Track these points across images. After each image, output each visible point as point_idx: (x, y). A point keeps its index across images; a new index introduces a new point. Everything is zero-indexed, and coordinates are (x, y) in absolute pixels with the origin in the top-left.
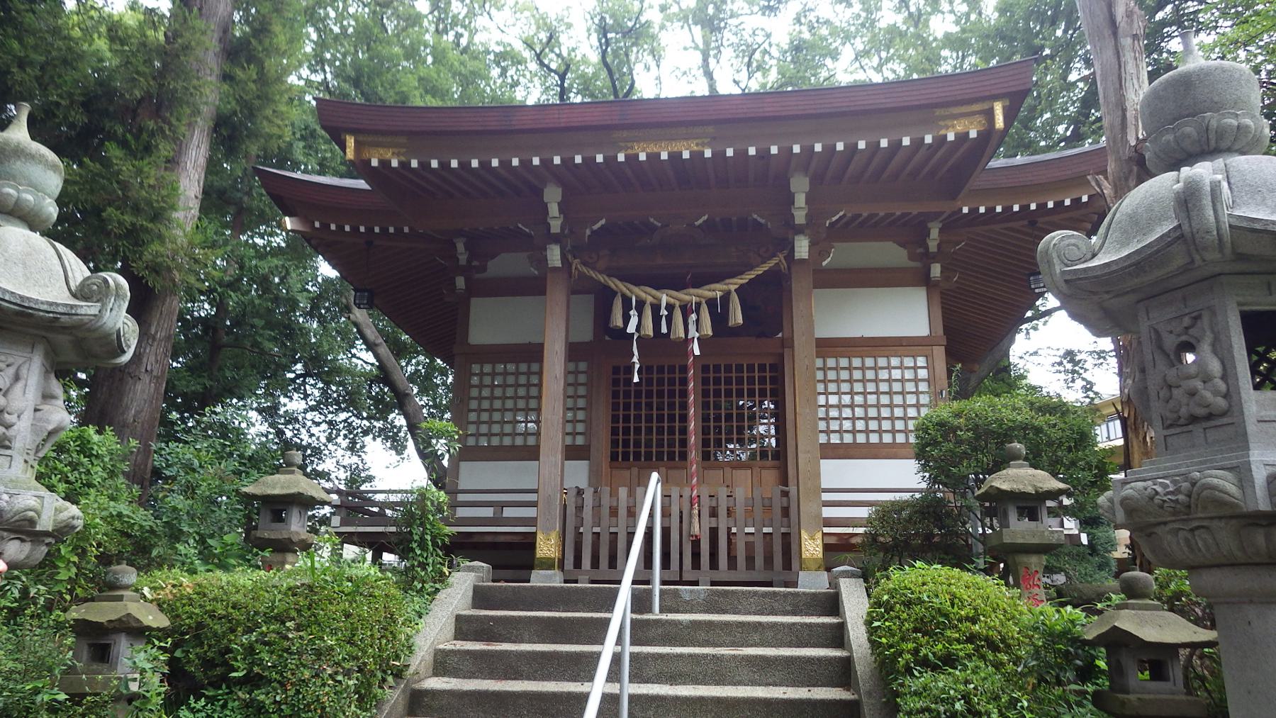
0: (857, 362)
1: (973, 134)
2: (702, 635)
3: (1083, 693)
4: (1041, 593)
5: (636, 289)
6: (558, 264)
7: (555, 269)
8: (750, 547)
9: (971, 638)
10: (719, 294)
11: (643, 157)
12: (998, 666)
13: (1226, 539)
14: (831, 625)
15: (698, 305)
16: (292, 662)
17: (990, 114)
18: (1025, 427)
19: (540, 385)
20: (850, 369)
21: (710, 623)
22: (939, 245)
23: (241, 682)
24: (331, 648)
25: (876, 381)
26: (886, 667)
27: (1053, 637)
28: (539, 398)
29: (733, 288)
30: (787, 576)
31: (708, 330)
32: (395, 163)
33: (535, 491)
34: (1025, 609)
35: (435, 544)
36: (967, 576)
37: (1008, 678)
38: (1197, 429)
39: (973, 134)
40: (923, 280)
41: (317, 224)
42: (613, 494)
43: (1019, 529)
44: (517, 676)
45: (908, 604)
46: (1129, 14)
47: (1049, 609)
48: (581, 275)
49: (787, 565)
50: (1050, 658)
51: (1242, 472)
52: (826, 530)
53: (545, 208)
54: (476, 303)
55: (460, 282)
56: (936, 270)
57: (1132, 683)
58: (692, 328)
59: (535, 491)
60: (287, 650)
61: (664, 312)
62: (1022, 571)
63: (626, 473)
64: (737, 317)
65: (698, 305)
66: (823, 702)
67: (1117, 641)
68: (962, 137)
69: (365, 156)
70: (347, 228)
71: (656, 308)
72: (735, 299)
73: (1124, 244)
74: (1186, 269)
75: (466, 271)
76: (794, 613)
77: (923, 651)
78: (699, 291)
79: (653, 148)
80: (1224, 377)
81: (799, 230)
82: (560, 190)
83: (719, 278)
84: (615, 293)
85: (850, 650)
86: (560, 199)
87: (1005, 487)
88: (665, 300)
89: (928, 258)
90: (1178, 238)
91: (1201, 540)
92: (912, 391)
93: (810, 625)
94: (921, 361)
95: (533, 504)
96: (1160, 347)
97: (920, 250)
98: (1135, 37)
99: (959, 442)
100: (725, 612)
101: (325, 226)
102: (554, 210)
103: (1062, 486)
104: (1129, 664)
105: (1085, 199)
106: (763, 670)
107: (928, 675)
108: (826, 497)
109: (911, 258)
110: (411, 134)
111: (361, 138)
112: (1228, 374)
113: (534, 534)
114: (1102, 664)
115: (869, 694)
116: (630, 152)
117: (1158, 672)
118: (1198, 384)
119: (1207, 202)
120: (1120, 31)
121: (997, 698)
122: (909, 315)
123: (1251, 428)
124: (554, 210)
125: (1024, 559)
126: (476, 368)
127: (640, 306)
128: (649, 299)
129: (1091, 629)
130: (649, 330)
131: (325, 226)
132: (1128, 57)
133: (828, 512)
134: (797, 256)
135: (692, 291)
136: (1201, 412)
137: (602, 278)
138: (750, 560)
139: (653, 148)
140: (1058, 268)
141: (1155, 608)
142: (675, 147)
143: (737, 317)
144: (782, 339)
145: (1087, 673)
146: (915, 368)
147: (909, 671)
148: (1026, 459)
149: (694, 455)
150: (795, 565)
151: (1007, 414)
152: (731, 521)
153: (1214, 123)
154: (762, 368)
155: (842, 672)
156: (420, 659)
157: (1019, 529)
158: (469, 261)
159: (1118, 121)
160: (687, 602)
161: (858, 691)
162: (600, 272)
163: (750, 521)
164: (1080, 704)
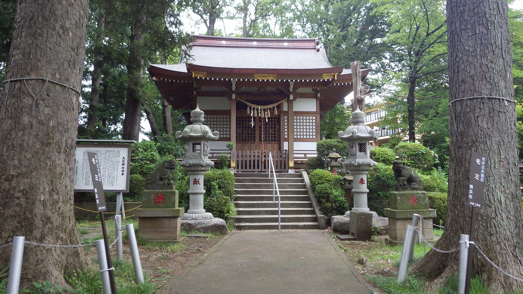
17: (334, 76)
18: (336, 146)
26: (313, 185)
30: (285, 170)
32: (203, 78)
40: (316, 97)
43: (334, 163)
47: (337, 176)
49: (285, 168)
51: (355, 161)
55: (195, 93)
61: (259, 111)
67: (345, 180)
69: (196, 76)
71: (258, 110)
72: (276, 109)
84: (247, 106)
88: (260, 108)
90: (351, 136)
94: (314, 118)
101: (164, 79)
108: (295, 152)
122: (310, 106)
127: (254, 109)
129: (342, 178)
131: (164, 79)
132: (358, 80)
133: (295, 156)
146: (312, 119)
149: (257, 139)
150: (287, 168)
151: (333, 143)
155: (304, 186)
157: (334, 163)
161: (307, 188)
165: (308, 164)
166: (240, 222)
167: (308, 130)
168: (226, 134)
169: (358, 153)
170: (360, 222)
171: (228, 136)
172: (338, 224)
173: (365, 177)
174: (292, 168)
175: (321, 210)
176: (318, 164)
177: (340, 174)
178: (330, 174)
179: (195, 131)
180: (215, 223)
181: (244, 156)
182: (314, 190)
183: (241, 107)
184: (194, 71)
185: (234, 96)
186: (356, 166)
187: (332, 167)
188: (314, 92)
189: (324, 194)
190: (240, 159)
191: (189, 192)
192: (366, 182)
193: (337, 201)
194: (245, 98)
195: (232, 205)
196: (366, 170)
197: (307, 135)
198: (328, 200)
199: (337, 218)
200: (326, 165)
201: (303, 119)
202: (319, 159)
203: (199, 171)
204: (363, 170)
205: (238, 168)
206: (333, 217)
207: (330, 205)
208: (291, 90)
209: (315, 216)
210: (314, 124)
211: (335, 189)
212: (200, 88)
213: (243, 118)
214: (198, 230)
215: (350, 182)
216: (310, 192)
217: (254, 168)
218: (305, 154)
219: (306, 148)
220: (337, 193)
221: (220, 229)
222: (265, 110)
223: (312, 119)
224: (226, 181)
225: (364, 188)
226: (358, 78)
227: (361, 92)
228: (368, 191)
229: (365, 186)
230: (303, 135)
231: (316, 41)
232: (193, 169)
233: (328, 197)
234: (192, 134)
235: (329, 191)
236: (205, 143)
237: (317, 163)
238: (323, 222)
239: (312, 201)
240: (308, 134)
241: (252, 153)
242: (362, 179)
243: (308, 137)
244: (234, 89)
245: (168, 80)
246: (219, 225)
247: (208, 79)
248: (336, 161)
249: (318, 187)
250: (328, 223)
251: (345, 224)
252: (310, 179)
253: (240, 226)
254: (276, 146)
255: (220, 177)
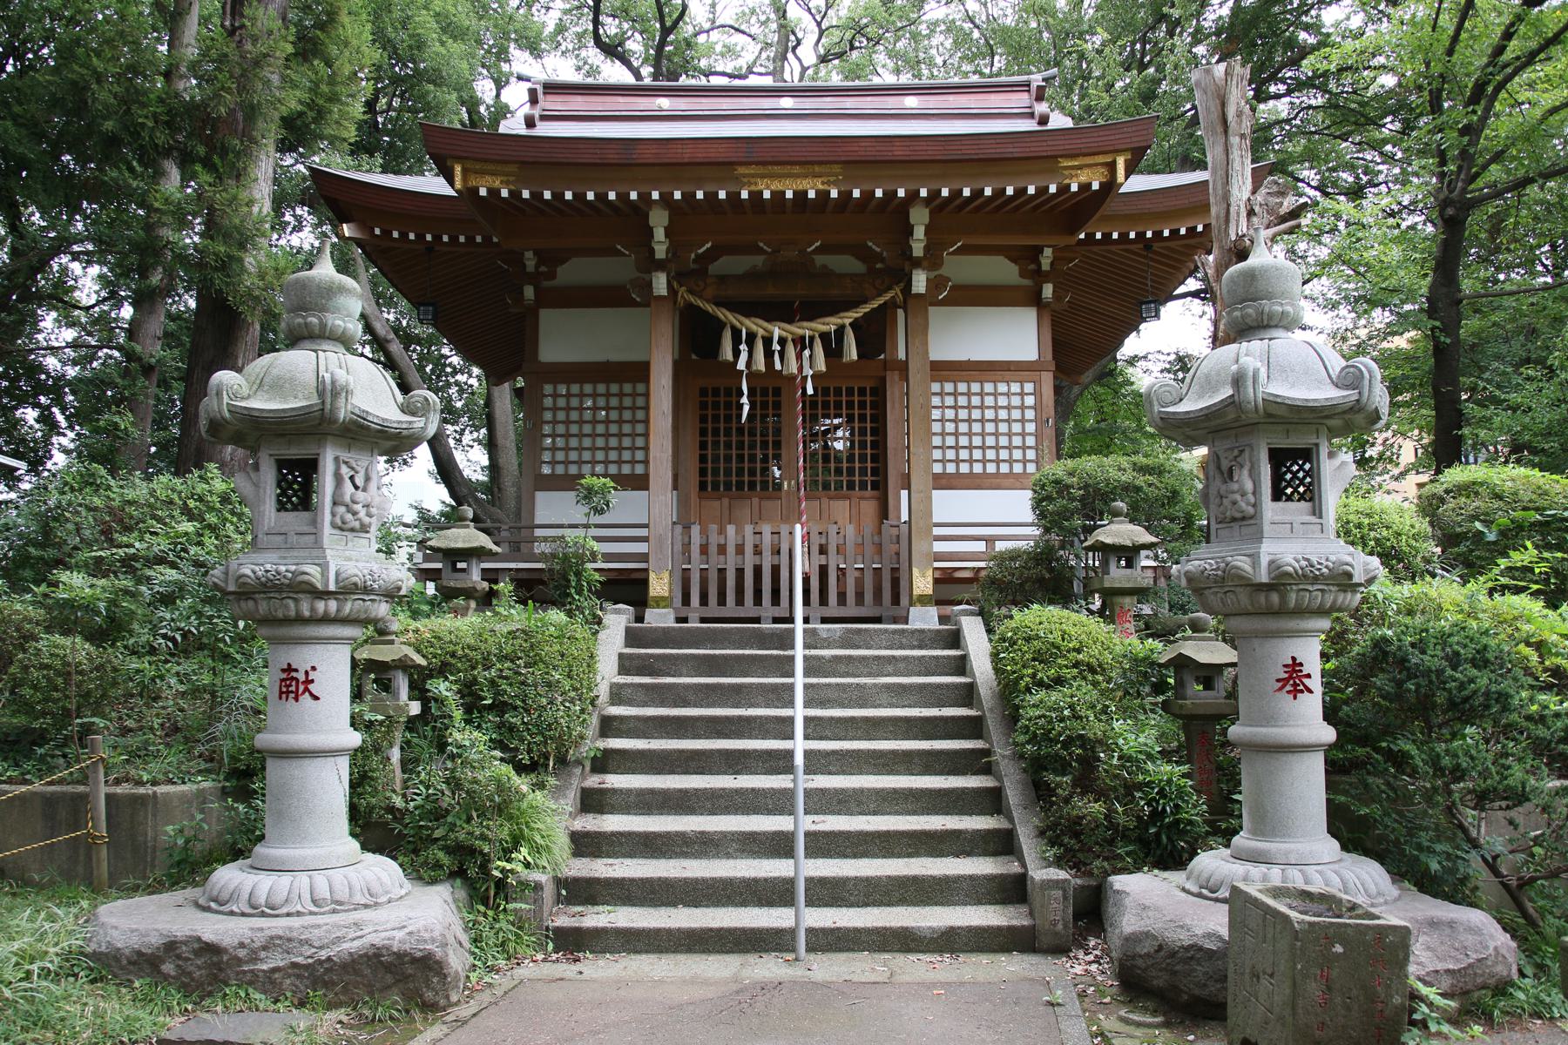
0: (962, 387)
1: (1095, 186)
2: (842, 668)
3: (1156, 704)
4: (1131, 627)
5: (747, 322)
6: (664, 292)
7: (660, 297)
8: (859, 583)
9: (1076, 665)
10: (833, 328)
11: (767, 195)
12: (1095, 684)
13: (1244, 598)
14: (954, 657)
15: (812, 339)
16: (531, 692)
18: (1129, 489)
19: (646, 421)
20: (955, 394)
21: (850, 657)
22: (1052, 264)
23: (490, 708)
24: (558, 682)
25: (982, 407)
26: (1009, 689)
27: (1136, 661)
28: (646, 435)
29: (847, 321)
30: (896, 611)
31: (821, 366)
32: (505, 193)
33: (646, 526)
34: (1117, 641)
35: (590, 590)
36: (1074, 616)
37: (1102, 693)
38: (1236, 525)
39: (1095, 186)
40: (1035, 300)
41: (377, 231)
42: (722, 531)
43: (1118, 575)
44: (686, 704)
45: (1028, 639)
46: (1239, 114)
48: (690, 306)
49: (896, 600)
50: (1133, 677)
51: (1254, 558)
52: (937, 565)
53: (650, 233)
54: (547, 317)
55: (529, 292)
56: (1048, 291)
57: (1189, 692)
58: (806, 363)
59: (646, 526)
60: (523, 683)
62: (1117, 610)
63: (716, 504)
64: (851, 353)
65: (812, 339)
66: (953, 718)
68: (1085, 187)
69: (472, 183)
70: (412, 236)
71: (768, 342)
73: (1201, 396)
74: (1237, 419)
75: (534, 279)
76: (920, 647)
77: (1040, 675)
78: (813, 325)
79: (777, 186)
80: (1254, 493)
81: (917, 263)
82: (666, 213)
83: (833, 312)
84: (720, 325)
85: (973, 676)
86: (666, 223)
87: (1108, 541)
88: (777, 333)
89: (1039, 276)
90: (1230, 403)
91: (1230, 598)
92: (1014, 417)
93: (936, 658)
94: (1029, 387)
95: (645, 539)
96: (1219, 468)
97: (1033, 267)
98: (1243, 136)
99: (1073, 499)
100: (859, 647)
101: (387, 233)
102: (659, 234)
103: (1154, 540)
104: (1188, 679)
105: (1200, 228)
106: (900, 694)
107: (1043, 693)
108: (937, 531)
109: (1022, 275)
110: (524, 164)
111: (469, 165)
112: (1256, 492)
113: (646, 570)
114: (1171, 681)
115: (991, 710)
116: (753, 188)
117: (1208, 684)
118: (1238, 497)
119: (1250, 383)
120: (1230, 131)
121: (1093, 707)
122: (1016, 336)
123: (1266, 528)
124: (659, 234)
125: (1119, 600)
126: (548, 389)
127: (751, 338)
128: (761, 332)
130: (760, 364)
131: (387, 233)
132: (1235, 154)
133: (939, 547)
134: (914, 290)
135: (805, 324)
136: (1238, 515)
137: (710, 308)
138: (860, 597)
139: (777, 186)
140: (1156, 408)
141: (1210, 639)
142: (802, 184)
143: (851, 353)
144: (885, 360)
145: (1159, 688)
147: (1028, 690)
148: (1127, 515)
150: (904, 601)
151: (1113, 474)
152: (841, 558)
153: (1267, 309)
154: (862, 392)
155: (968, 695)
156: (603, 691)
157: (1118, 575)
158: (537, 266)
159: (1223, 214)
160: (825, 640)
161: (980, 707)
162: (708, 301)
163: (860, 558)
164: (1153, 711)
165: (993, 582)
166: (592, 900)
167: (1004, 441)
168: (633, 462)
169: (1271, 510)
170: (1314, 989)
171: (639, 469)
172: (1146, 948)
173: (1309, 653)
174: (924, 600)
175: (1050, 834)
176: (1041, 581)
177: (1150, 629)
178: (1097, 627)
179: (277, 386)
180: (378, 939)
181: (713, 549)
182: (1012, 717)
183: (699, 338)
184: (459, 159)
185: (660, 283)
186: (1261, 587)
187: (1109, 594)
188: (1026, 282)
189: (1067, 744)
190: (696, 565)
191: (263, 740)
192: (1316, 683)
193: (1140, 786)
194: (710, 292)
195: (553, 813)
196: (1322, 612)
197: (998, 461)
198: (1086, 782)
199: (1150, 900)
200: (1077, 587)
201: (982, 394)
202: (1043, 556)
203: (300, 620)
204: (1302, 612)
205: (686, 601)
206: (1119, 882)
207: (1097, 808)
208: (918, 249)
209: (1015, 868)
210: (1030, 414)
211: (1126, 712)
212: (552, 275)
213: (716, 392)
214: (270, 984)
215: (1207, 675)
216: (993, 725)
217: (758, 600)
218: (990, 540)
219: (983, 516)
220: (1136, 736)
221: (403, 979)
222: (801, 343)
223: (1022, 394)
224: (534, 675)
225: (1307, 719)
226: (1235, 140)
227: (1251, 213)
228: (1329, 734)
229: (1312, 704)
230: (984, 461)
231: (1034, 85)
232: (283, 609)
233: (1089, 763)
234: (259, 403)
235: (1096, 729)
236: (344, 455)
237: (1040, 577)
238: (1057, 913)
239: (999, 778)
240: (1004, 454)
241: (742, 535)
242: (1295, 666)
243: (1004, 468)
244: (661, 251)
245: (404, 235)
246: (400, 955)
247: (526, 194)
248: (1129, 565)
249: (1037, 704)
250: (1092, 911)
251: (1195, 953)
252: (995, 656)
253: (578, 931)
254: (869, 507)
255: (508, 649)
